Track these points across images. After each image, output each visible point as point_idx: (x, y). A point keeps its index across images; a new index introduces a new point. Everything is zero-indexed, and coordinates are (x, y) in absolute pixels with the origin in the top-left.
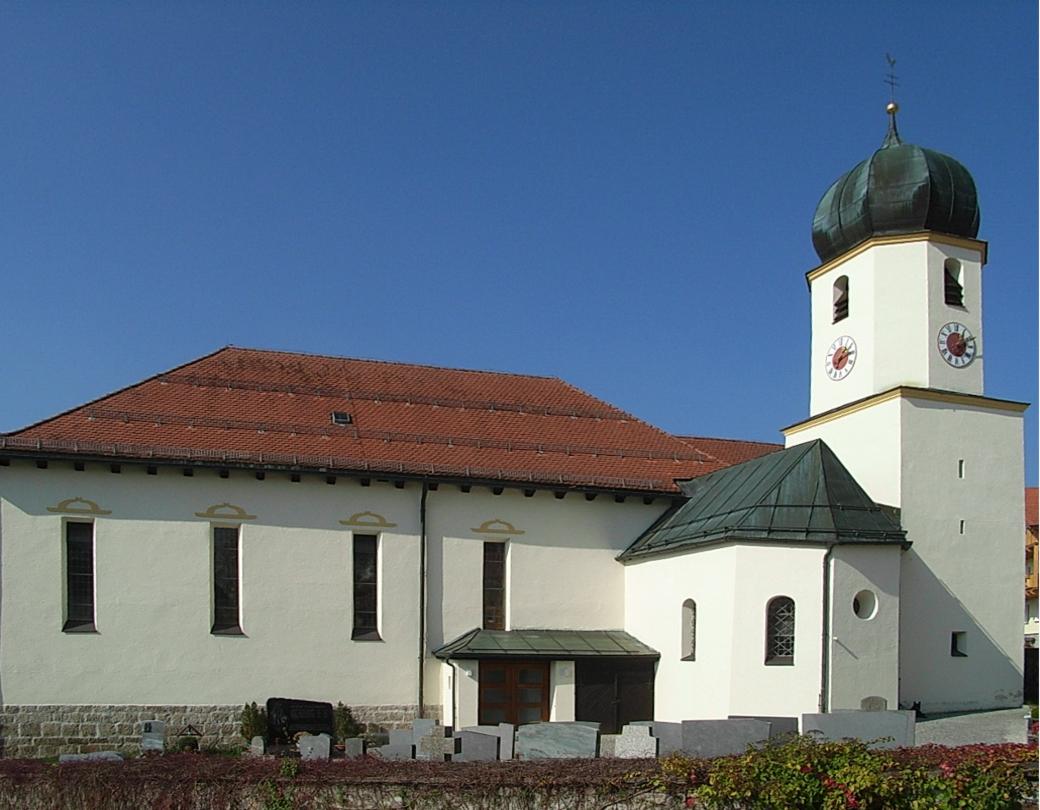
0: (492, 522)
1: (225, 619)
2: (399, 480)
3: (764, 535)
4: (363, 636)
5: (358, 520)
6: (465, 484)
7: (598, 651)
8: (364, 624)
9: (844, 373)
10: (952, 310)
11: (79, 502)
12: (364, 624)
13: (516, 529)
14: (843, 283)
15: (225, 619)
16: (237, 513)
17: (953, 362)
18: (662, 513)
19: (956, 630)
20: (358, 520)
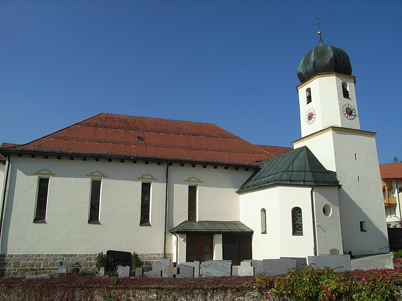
0: (94, 172)
1: (94, 218)
2: (159, 161)
3: (289, 182)
4: (37, 222)
6: (182, 163)
8: (145, 220)
10: (346, 99)
12: (145, 220)
15: (94, 218)
16: (197, 181)
17: (348, 118)
20: (144, 177)
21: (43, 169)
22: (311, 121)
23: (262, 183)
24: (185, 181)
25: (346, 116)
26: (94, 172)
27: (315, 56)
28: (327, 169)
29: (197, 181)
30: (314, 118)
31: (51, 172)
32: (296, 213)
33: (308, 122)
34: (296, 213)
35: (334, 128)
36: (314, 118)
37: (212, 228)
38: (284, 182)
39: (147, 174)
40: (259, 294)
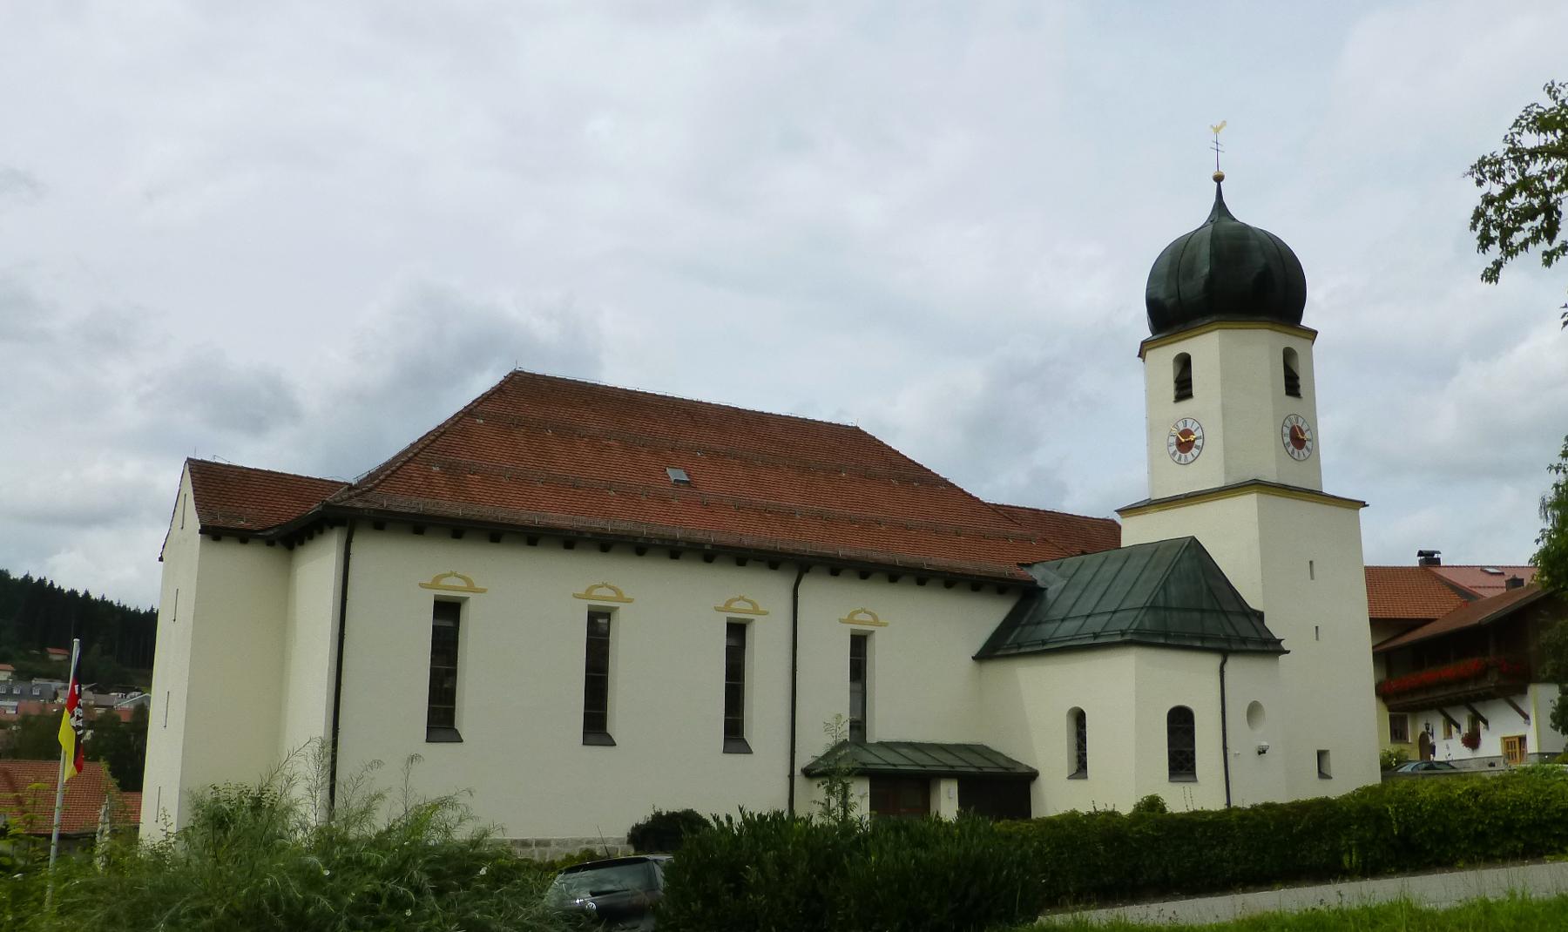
0: (446, 576)
1: (596, 726)
2: (773, 560)
3: (1198, 644)
4: (989, 768)
5: (594, 593)
6: (836, 567)
7: (894, 765)
8: (734, 735)
9: (1190, 458)
10: (1291, 399)
11: (741, 601)
12: (734, 735)
13: (477, 586)
14: (1184, 363)
15: (596, 726)
16: (615, 595)
17: (1296, 456)
18: (1388, 637)
19: (1323, 748)
20: (594, 593)
21: (449, 572)
22: (1189, 454)
23: (1068, 638)
24: (574, 596)
25: (1290, 449)
26: (446, 576)
27: (1273, 245)
28: (1251, 607)
29: (615, 595)
30: (1197, 447)
31: (876, 616)
32: (1181, 722)
33: (1177, 456)
34: (1181, 722)
35: (1256, 485)
36: (1197, 447)
37: (927, 762)
38: (1251, 647)
39: (742, 598)
40: (1125, 919)
